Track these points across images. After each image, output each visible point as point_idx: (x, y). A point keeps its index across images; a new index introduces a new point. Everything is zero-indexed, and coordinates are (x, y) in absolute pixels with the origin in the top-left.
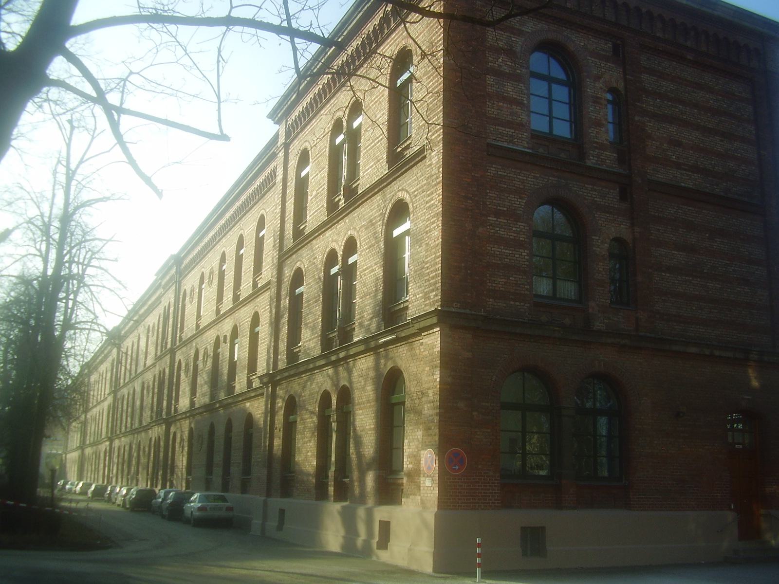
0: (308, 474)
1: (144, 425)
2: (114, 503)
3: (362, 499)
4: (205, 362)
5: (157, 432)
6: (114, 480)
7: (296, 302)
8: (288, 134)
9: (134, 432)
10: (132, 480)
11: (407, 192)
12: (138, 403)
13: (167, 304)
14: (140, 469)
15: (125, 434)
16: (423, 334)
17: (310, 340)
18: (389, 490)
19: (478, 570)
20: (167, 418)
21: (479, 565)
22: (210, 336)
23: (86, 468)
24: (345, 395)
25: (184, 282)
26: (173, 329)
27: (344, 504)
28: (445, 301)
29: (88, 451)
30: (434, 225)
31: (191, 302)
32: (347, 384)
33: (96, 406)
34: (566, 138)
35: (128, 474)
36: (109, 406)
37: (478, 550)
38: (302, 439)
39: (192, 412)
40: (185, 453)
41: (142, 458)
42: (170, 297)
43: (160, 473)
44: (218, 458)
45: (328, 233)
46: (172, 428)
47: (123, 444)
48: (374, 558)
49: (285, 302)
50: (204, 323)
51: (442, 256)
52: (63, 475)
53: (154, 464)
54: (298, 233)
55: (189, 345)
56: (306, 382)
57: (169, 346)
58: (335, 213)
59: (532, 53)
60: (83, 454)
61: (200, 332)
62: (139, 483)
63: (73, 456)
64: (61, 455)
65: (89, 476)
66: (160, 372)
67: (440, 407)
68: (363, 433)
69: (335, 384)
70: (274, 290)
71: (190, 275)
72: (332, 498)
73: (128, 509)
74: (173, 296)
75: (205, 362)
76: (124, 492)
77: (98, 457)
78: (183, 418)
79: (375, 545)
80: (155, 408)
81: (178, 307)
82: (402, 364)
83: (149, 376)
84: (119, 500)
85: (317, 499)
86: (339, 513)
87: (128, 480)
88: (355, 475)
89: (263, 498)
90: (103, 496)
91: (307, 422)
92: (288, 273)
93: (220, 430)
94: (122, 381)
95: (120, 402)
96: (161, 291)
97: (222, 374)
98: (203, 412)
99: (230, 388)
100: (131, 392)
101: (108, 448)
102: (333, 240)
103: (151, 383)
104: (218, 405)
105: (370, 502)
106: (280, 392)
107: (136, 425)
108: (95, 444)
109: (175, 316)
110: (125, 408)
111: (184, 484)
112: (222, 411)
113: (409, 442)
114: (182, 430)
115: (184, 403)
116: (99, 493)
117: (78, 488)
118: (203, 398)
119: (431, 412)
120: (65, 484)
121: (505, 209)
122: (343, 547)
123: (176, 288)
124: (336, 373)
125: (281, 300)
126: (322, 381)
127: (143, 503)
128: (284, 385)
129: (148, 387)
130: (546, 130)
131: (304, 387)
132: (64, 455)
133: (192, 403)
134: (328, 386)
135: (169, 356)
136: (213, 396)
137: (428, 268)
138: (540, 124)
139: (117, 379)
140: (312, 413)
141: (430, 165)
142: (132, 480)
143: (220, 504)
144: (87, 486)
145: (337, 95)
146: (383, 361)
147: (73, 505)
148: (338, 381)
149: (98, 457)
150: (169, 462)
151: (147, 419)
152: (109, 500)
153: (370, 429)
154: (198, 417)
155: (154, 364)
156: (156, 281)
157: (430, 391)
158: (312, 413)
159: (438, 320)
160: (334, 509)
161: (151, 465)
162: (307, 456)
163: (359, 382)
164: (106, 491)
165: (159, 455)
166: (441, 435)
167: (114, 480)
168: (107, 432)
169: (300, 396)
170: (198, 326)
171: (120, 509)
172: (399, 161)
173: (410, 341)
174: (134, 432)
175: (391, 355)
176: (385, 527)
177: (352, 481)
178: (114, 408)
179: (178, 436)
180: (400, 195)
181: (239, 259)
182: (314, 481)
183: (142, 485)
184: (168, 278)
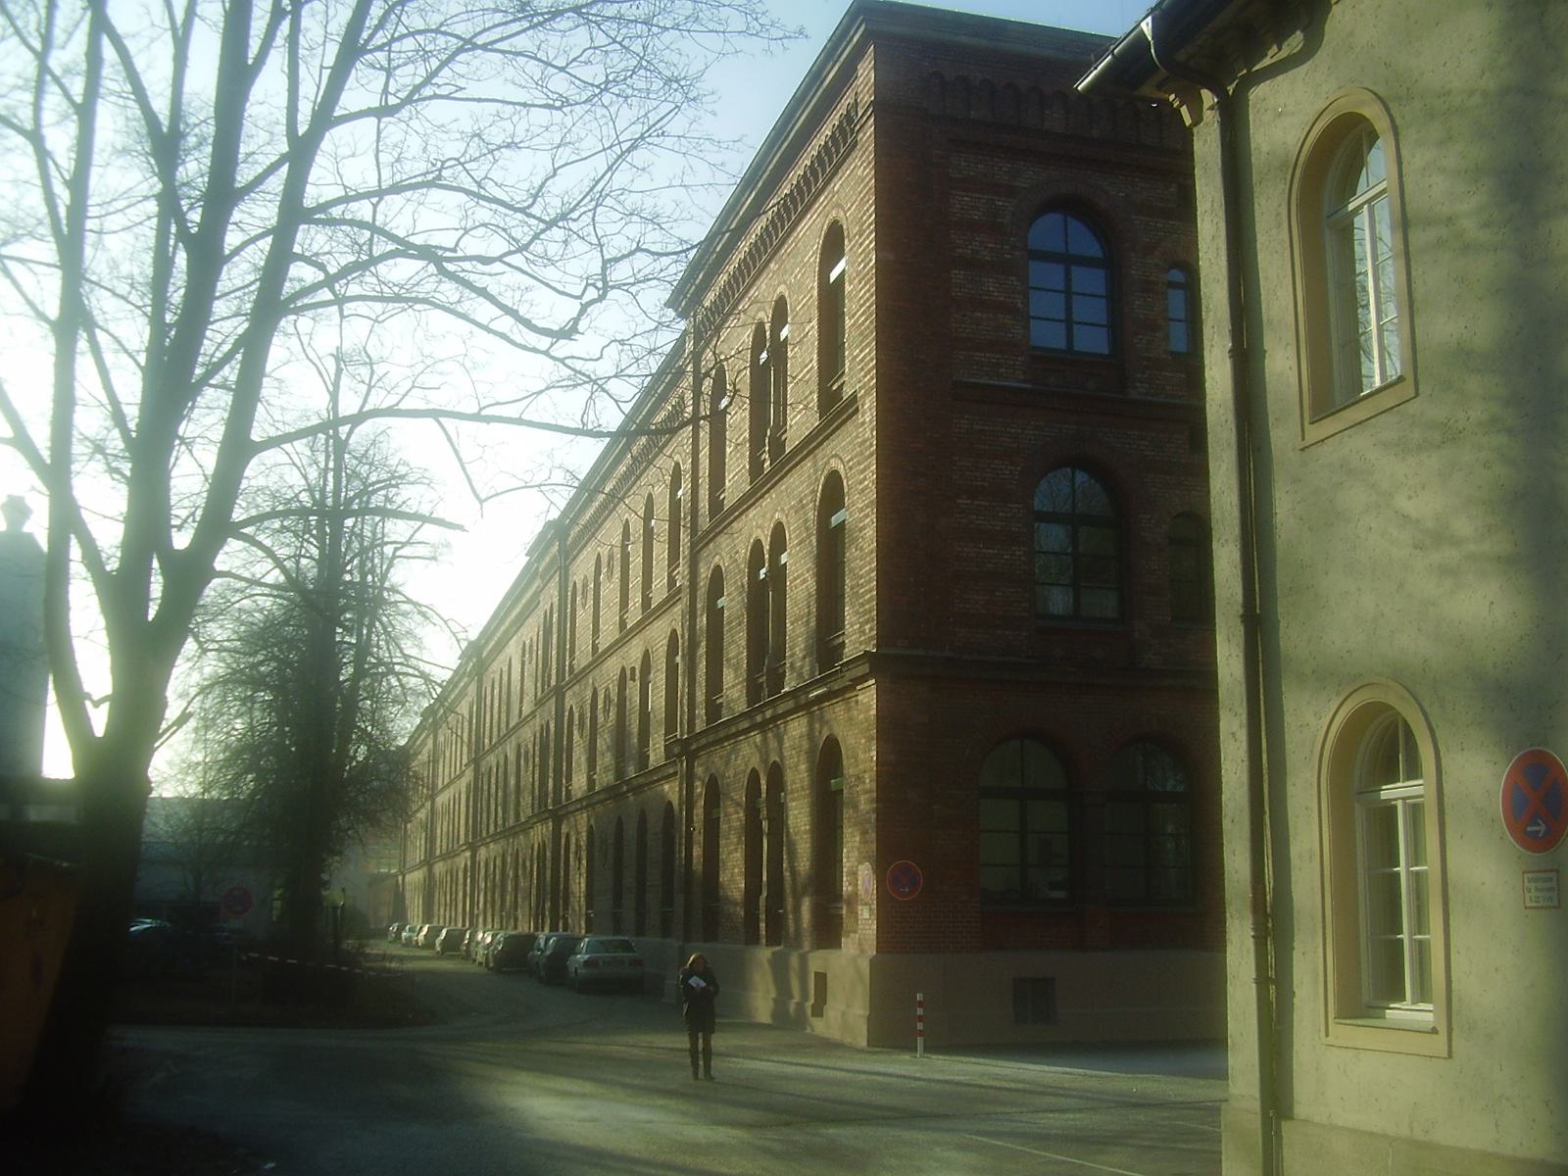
0: (736, 904)
1: (523, 820)
2: (475, 960)
3: (798, 945)
4: (606, 711)
5: (541, 832)
6: (481, 919)
7: (716, 616)
8: (698, 336)
9: (507, 833)
10: (508, 919)
11: (841, 459)
12: (512, 782)
13: (548, 607)
14: (519, 900)
15: (495, 838)
16: (858, 688)
17: (733, 686)
18: (829, 931)
19: (920, 1041)
20: (556, 811)
21: (921, 1033)
22: (612, 667)
23: (436, 899)
24: (776, 773)
25: (573, 568)
26: (558, 653)
27: (777, 948)
28: (882, 638)
29: (439, 868)
30: (868, 520)
31: (584, 605)
32: (777, 759)
33: (448, 786)
34: (1102, 355)
35: (502, 910)
36: (468, 787)
37: (920, 1011)
38: (727, 846)
39: (590, 800)
40: (583, 870)
41: (521, 879)
42: (551, 595)
43: (548, 905)
44: (629, 879)
45: (752, 513)
46: (563, 826)
47: (492, 855)
48: (808, 1030)
49: (702, 621)
50: (604, 643)
51: (878, 569)
52: (400, 914)
53: (538, 890)
54: (716, 505)
55: (583, 682)
56: (730, 754)
57: (553, 682)
58: (762, 482)
59: (1031, 225)
60: (430, 874)
61: (599, 658)
62: (519, 924)
63: (416, 877)
64: (395, 876)
65: (441, 912)
66: (542, 726)
67: (878, 800)
68: (798, 838)
69: (764, 760)
70: (686, 600)
71: (581, 557)
72: (764, 940)
73: (492, 968)
74: (556, 593)
75: (606, 711)
76: (489, 940)
77: (454, 880)
78: (577, 810)
79: (809, 1011)
80: (537, 791)
81: (566, 614)
82: (840, 732)
83: (528, 734)
84: (480, 958)
85: (747, 943)
86: (769, 961)
87: (501, 917)
88: (789, 902)
89: (681, 943)
90: (459, 950)
91: (733, 818)
92: (705, 573)
93: (631, 831)
94: (487, 741)
95: (485, 779)
96: (537, 583)
97: (631, 733)
98: (606, 800)
99: (643, 758)
100: (502, 762)
101: (469, 863)
102: (756, 525)
103: (530, 746)
104: (625, 788)
105: (807, 945)
106: (699, 770)
107: (511, 822)
108: (450, 855)
109: (560, 630)
110: (493, 790)
111: (583, 924)
112: (632, 798)
113: (848, 852)
114: (579, 827)
115: (579, 783)
116: (453, 944)
117: (421, 937)
118: (605, 778)
119: (868, 807)
120: (400, 930)
121: (986, 484)
122: (775, 1015)
123: (560, 582)
124: (765, 740)
125: (696, 618)
126: (746, 755)
127: (514, 957)
128: (704, 759)
129: (527, 753)
130: (1062, 344)
131: (727, 763)
132: (400, 878)
133: (591, 782)
134: (755, 762)
135: (554, 699)
136: (620, 772)
137: (862, 586)
138: (1048, 336)
139: (479, 739)
140: (738, 804)
141: (863, 423)
142: (508, 919)
143: (620, 954)
144: (434, 932)
145: (758, 283)
146: (817, 726)
147: (394, 965)
148: (767, 755)
149: (454, 880)
150: (562, 886)
151: (526, 812)
152: (468, 956)
153: (805, 832)
154: (599, 808)
155: (533, 712)
156: (529, 564)
157: (866, 776)
158: (738, 804)
159: (871, 669)
160: (764, 954)
161: (534, 891)
162: (733, 877)
163: (791, 757)
164: (463, 940)
165: (545, 873)
166: (880, 841)
167: (481, 919)
168: (466, 835)
169: (723, 777)
170: (595, 647)
171: (483, 970)
172: (834, 409)
173: (847, 696)
174: (507, 833)
175: (827, 717)
176: (821, 978)
177: (785, 913)
178: (475, 789)
179: (573, 840)
180: (835, 464)
181: (648, 535)
182: (742, 913)
183: (525, 927)
184: (547, 559)
